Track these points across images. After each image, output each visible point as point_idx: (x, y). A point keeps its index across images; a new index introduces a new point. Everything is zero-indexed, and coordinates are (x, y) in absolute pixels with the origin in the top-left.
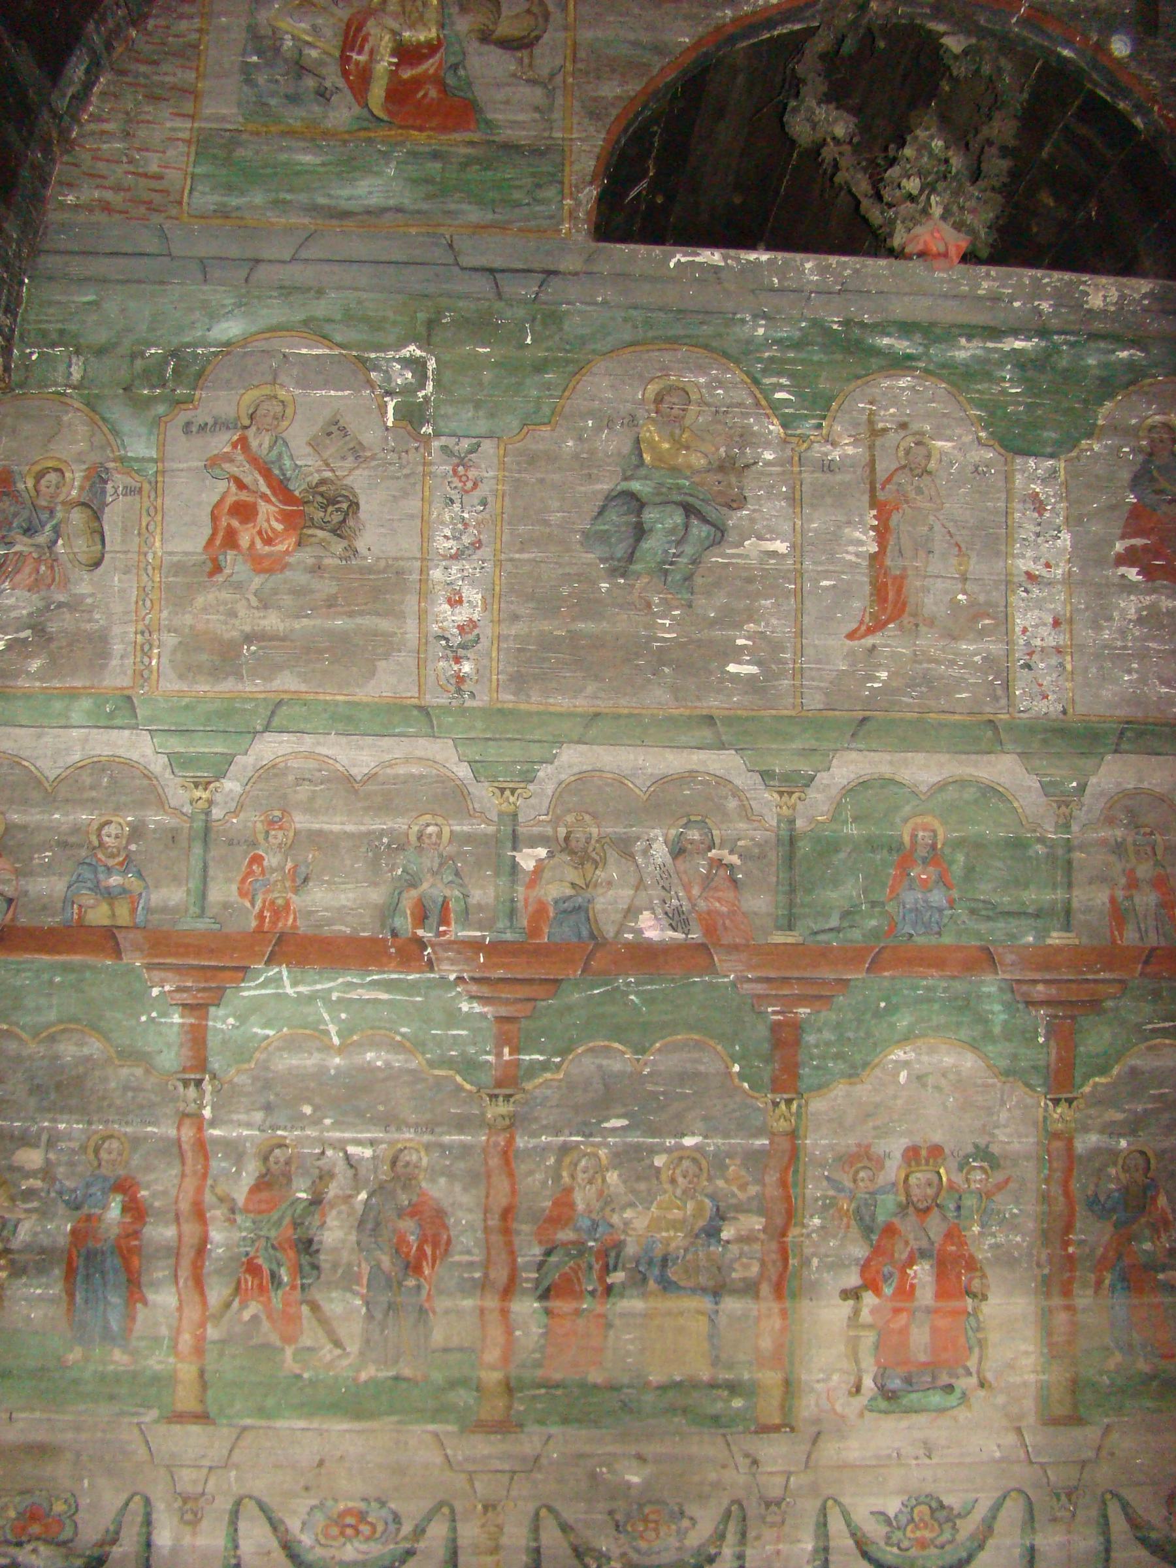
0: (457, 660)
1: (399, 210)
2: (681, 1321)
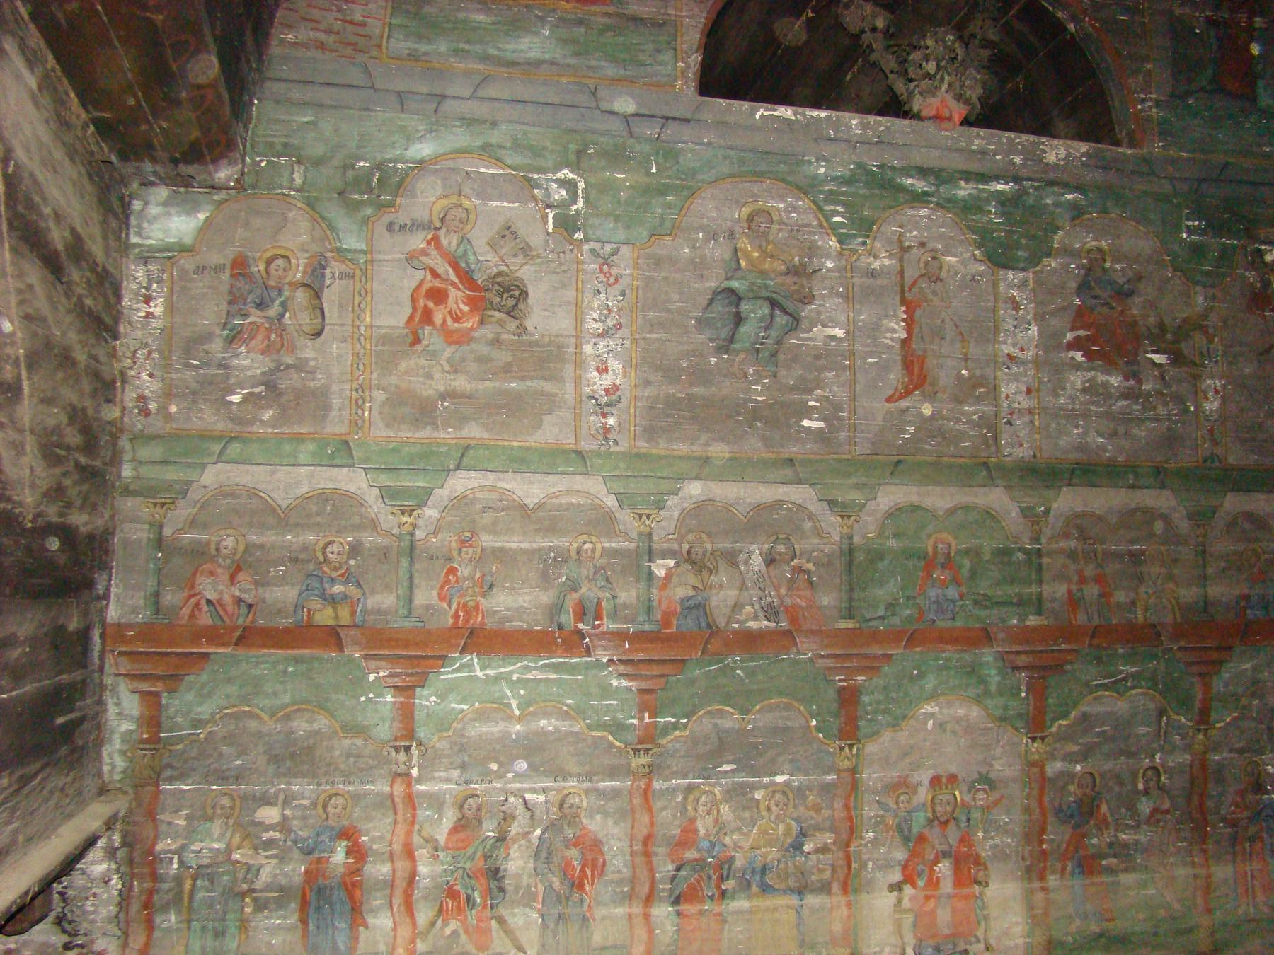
0: (604, 415)
1: (553, 63)
2: (777, 915)
